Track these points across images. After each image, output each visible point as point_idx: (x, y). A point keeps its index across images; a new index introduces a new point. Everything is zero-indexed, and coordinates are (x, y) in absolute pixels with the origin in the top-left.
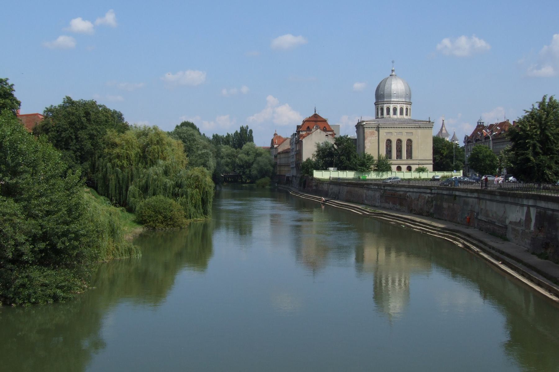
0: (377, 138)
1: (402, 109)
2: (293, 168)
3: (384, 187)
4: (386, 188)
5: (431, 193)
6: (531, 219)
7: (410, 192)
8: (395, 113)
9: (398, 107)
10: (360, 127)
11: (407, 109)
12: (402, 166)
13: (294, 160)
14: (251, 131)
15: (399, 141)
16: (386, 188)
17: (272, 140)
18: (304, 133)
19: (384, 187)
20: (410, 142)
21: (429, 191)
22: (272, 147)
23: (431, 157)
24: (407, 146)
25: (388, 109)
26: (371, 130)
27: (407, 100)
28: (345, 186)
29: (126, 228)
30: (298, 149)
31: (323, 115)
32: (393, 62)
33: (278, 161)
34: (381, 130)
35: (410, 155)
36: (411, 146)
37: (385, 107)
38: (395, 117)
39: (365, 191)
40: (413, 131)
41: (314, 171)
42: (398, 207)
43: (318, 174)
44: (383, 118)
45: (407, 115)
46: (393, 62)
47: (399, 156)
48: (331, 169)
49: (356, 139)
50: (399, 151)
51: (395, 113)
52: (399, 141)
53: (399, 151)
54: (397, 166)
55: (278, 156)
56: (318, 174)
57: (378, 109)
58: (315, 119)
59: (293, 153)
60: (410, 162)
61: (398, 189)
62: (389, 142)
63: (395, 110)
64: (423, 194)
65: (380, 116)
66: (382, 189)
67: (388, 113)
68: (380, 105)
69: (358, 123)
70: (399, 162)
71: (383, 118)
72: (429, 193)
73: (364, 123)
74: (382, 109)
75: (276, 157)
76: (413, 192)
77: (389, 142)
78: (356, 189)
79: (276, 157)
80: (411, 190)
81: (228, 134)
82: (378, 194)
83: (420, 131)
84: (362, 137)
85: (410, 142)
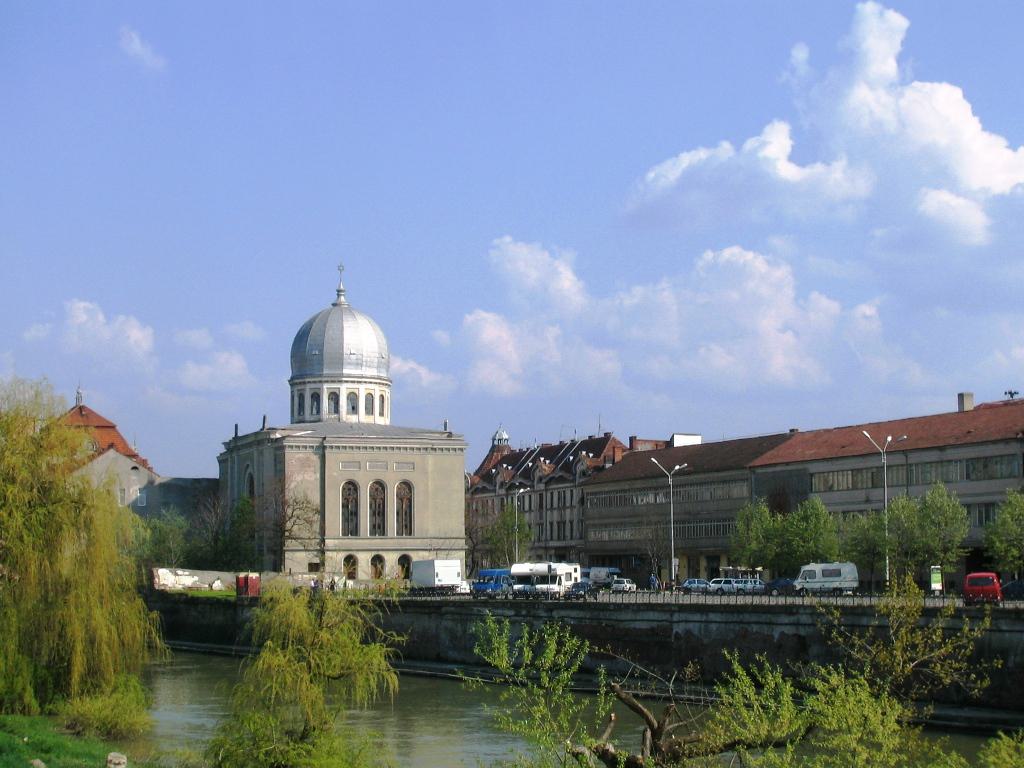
1: (370, 398)
9: (362, 391)
11: (382, 397)
12: (384, 555)
15: (379, 487)
20: (407, 487)
23: (461, 530)
24: (400, 499)
25: (335, 397)
26: (301, 454)
27: (383, 374)
29: (835, 743)
32: (340, 269)
34: (327, 451)
35: (406, 526)
36: (410, 500)
38: (353, 419)
40: (415, 457)
44: (319, 420)
46: (340, 269)
47: (379, 528)
50: (379, 512)
52: (379, 487)
53: (379, 512)
54: (374, 553)
57: (302, 397)
60: (407, 542)
62: (352, 487)
63: (353, 398)
65: (307, 415)
68: (308, 386)
70: (378, 542)
77: (352, 487)
81: (224, 444)
83: (431, 460)
85: (407, 487)
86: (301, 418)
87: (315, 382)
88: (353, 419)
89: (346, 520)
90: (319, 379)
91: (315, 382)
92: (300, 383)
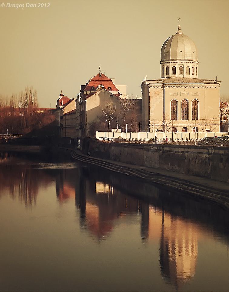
0: (162, 98)
2: (78, 130)
3: (163, 148)
4: (165, 148)
5: (208, 153)
6: (130, 131)
7: (187, 152)
8: (181, 73)
9: (185, 66)
10: (145, 87)
13: (78, 122)
14: (36, 92)
16: (165, 148)
17: (58, 100)
18: (88, 93)
19: (163, 148)
21: (206, 151)
22: (58, 108)
25: (174, 69)
26: (156, 90)
28: (126, 147)
30: (82, 109)
31: (108, 75)
32: (179, 20)
33: (64, 123)
35: (196, 116)
37: (171, 66)
38: (181, 76)
39: (145, 152)
41: (97, 132)
42: (177, 168)
43: (99, 135)
44: (169, 77)
45: (193, 74)
46: (179, 20)
48: (114, 130)
49: (141, 100)
51: (181, 73)
55: (64, 117)
56: (99, 135)
57: (163, 68)
58: (99, 79)
59: (78, 114)
61: (177, 150)
63: (181, 69)
64: (200, 155)
66: (161, 150)
67: (174, 72)
69: (143, 83)
70: (185, 122)
71: (169, 77)
72: (206, 153)
73: (149, 82)
74: (168, 68)
75: (61, 118)
76: (191, 152)
77: (174, 103)
78: (137, 150)
79: (61, 118)
80: (189, 150)
82: (157, 155)
84: (146, 97)
85: (196, 104)
86: (163, 76)
87: (167, 63)
88: (181, 76)
89: (172, 114)
90: (176, 61)
91: (167, 63)
92: (163, 63)
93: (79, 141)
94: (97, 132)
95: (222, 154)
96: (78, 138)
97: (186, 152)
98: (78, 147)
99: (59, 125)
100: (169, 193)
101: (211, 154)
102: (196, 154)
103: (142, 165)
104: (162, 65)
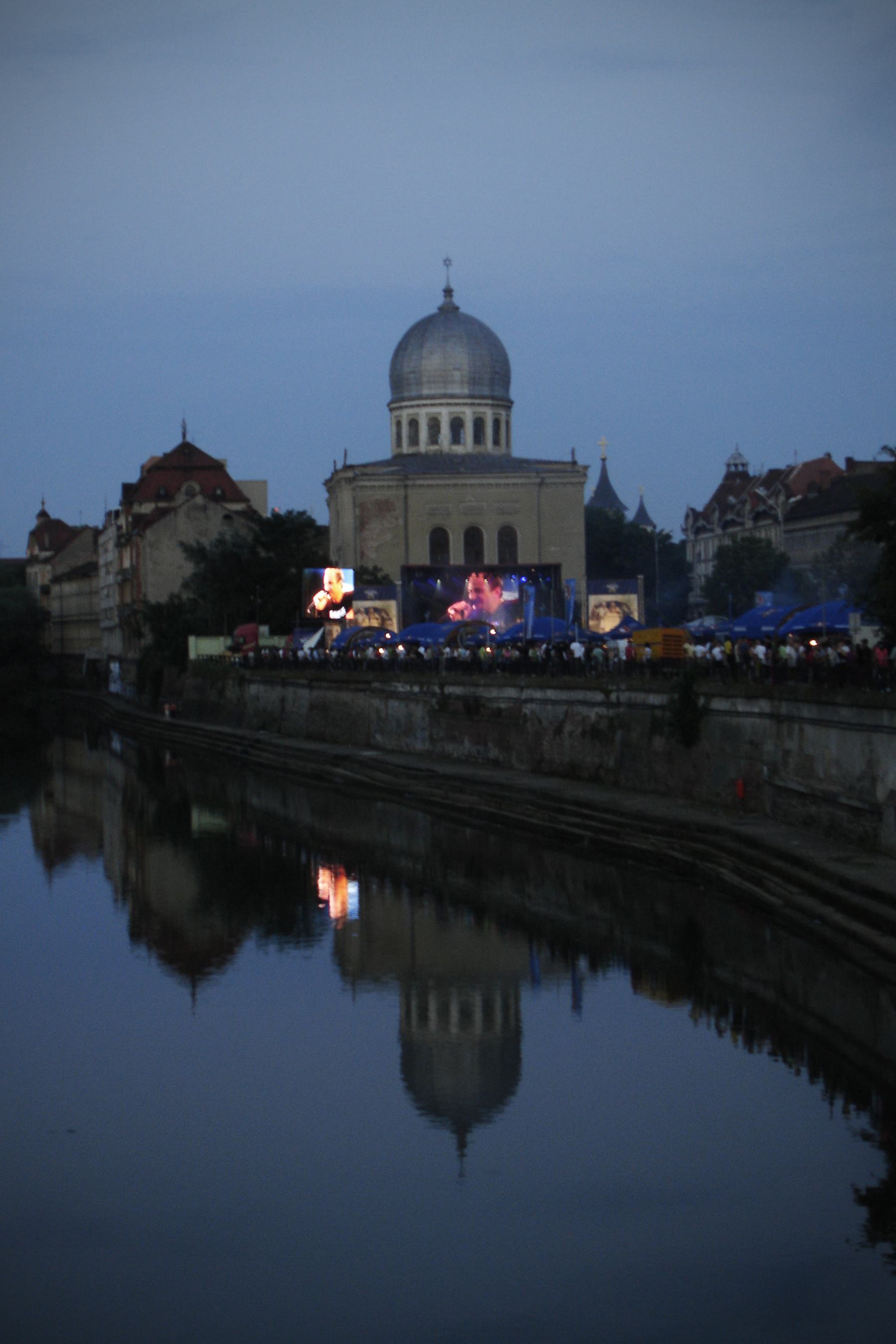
2: (110, 629)
3: (442, 687)
5: (607, 704)
7: (531, 700)
8: (456, 438)
19: (442, 687)
33: (54, 607)
41: (192, 640)
51: (456, 438)
57: (399, 424)
63: (434, 425)
66: (434, 694)
72: (600, 704)
76: (545, 702)
87: (412, 406)
88: (459, 449)
91: (412, 406)
93: (115, 667)
94: (192, 640)
95: (661, 707)
96: (111, 658)
97: (526, 701)
98: (114, 687)
99: (655, 699)
100: (468, 831)
101: (618, 704)
102: (564, 708)
103: (369, 746)
104: (396, 413)
